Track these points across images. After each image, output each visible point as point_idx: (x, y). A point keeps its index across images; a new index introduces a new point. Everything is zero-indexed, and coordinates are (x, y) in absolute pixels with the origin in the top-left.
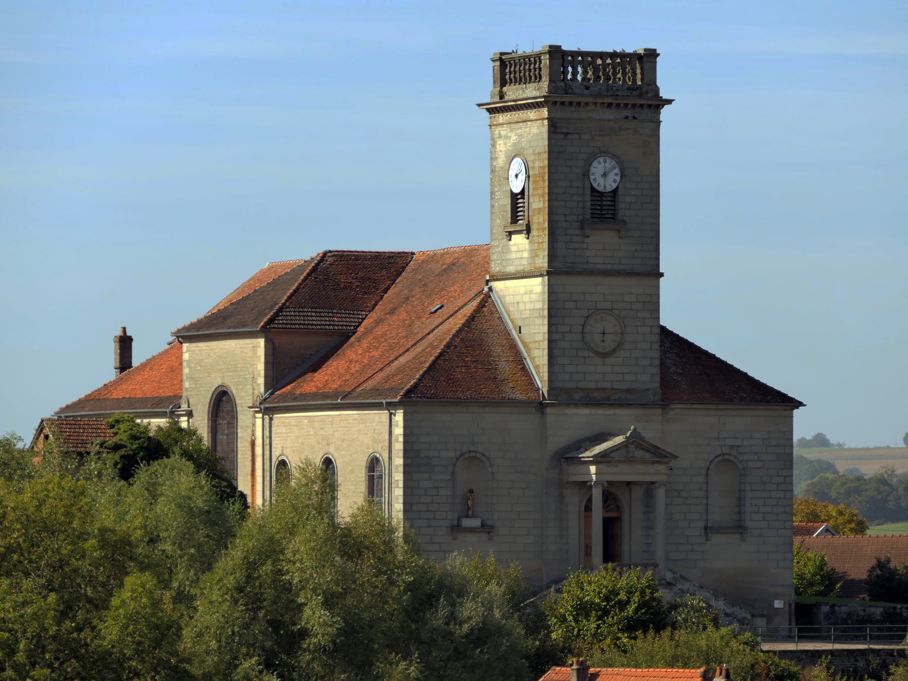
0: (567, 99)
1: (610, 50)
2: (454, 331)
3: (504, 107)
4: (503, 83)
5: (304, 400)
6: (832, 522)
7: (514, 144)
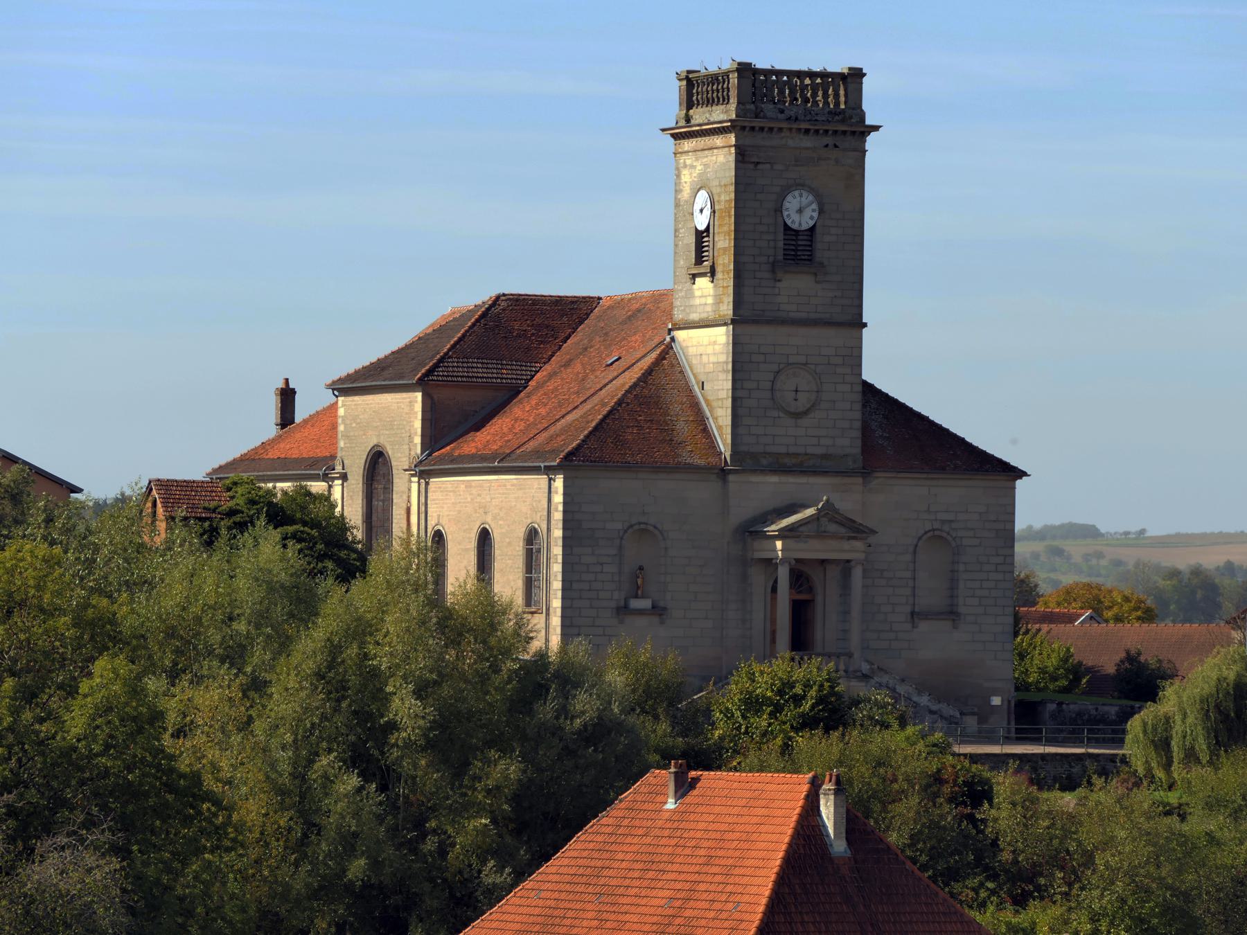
0: (757, 123)
1: (805, 68)
2: (627, 387)
3: (689, 132)
4: (689, 107)
5: (462, 462)
6: (1115, 610)
7: (700, 175)
